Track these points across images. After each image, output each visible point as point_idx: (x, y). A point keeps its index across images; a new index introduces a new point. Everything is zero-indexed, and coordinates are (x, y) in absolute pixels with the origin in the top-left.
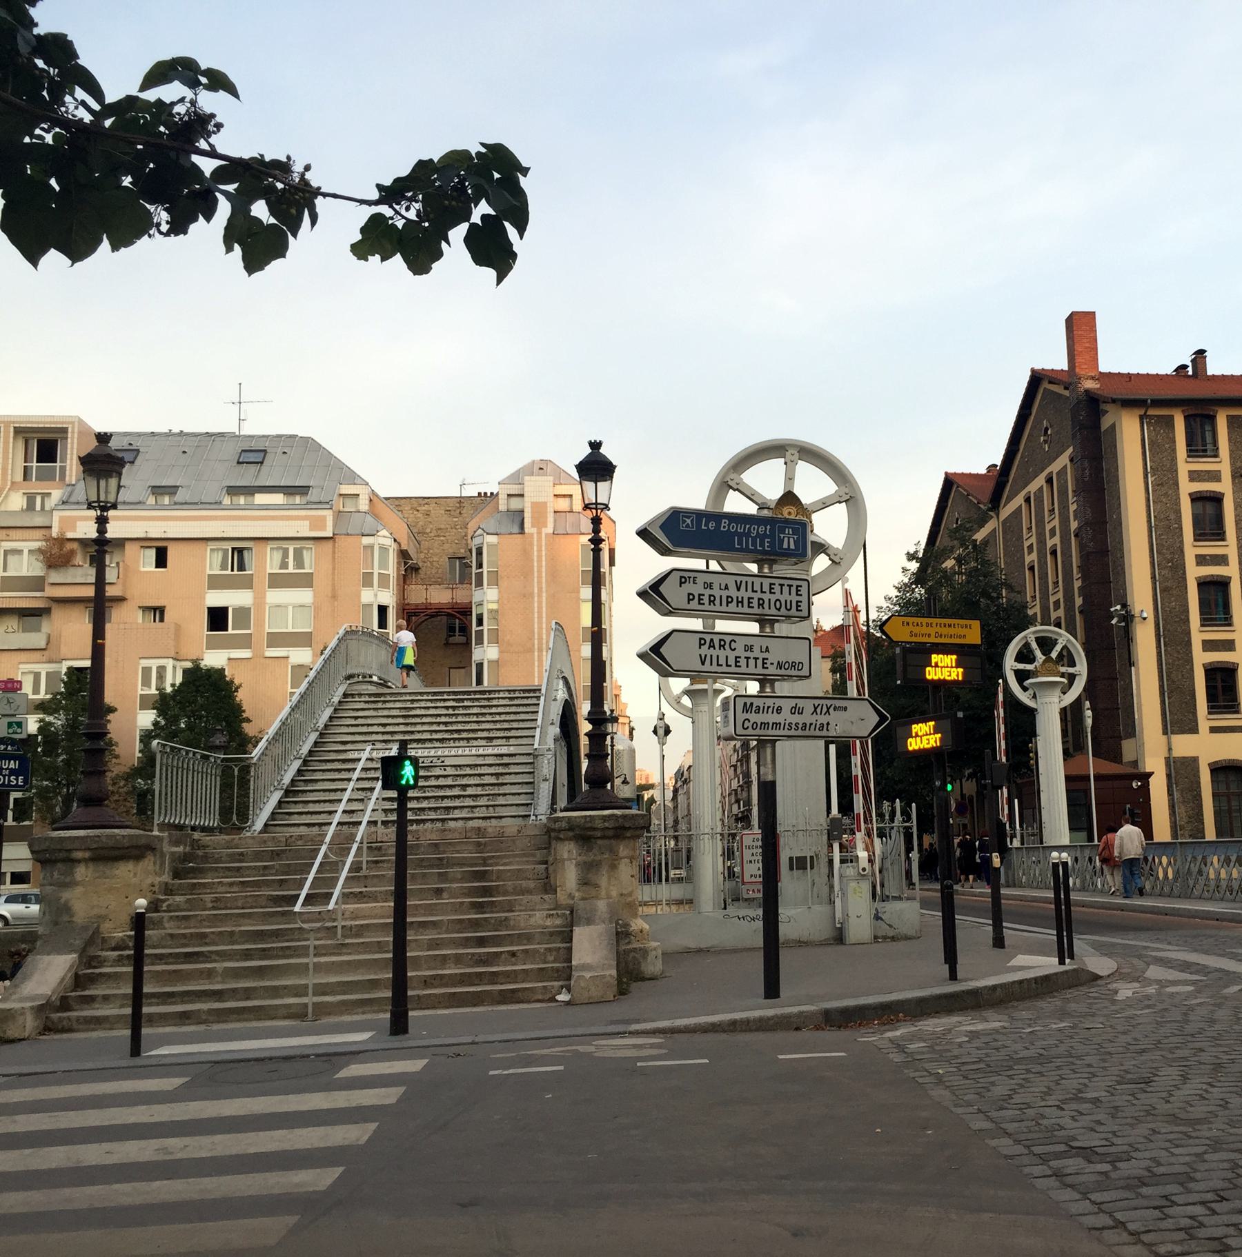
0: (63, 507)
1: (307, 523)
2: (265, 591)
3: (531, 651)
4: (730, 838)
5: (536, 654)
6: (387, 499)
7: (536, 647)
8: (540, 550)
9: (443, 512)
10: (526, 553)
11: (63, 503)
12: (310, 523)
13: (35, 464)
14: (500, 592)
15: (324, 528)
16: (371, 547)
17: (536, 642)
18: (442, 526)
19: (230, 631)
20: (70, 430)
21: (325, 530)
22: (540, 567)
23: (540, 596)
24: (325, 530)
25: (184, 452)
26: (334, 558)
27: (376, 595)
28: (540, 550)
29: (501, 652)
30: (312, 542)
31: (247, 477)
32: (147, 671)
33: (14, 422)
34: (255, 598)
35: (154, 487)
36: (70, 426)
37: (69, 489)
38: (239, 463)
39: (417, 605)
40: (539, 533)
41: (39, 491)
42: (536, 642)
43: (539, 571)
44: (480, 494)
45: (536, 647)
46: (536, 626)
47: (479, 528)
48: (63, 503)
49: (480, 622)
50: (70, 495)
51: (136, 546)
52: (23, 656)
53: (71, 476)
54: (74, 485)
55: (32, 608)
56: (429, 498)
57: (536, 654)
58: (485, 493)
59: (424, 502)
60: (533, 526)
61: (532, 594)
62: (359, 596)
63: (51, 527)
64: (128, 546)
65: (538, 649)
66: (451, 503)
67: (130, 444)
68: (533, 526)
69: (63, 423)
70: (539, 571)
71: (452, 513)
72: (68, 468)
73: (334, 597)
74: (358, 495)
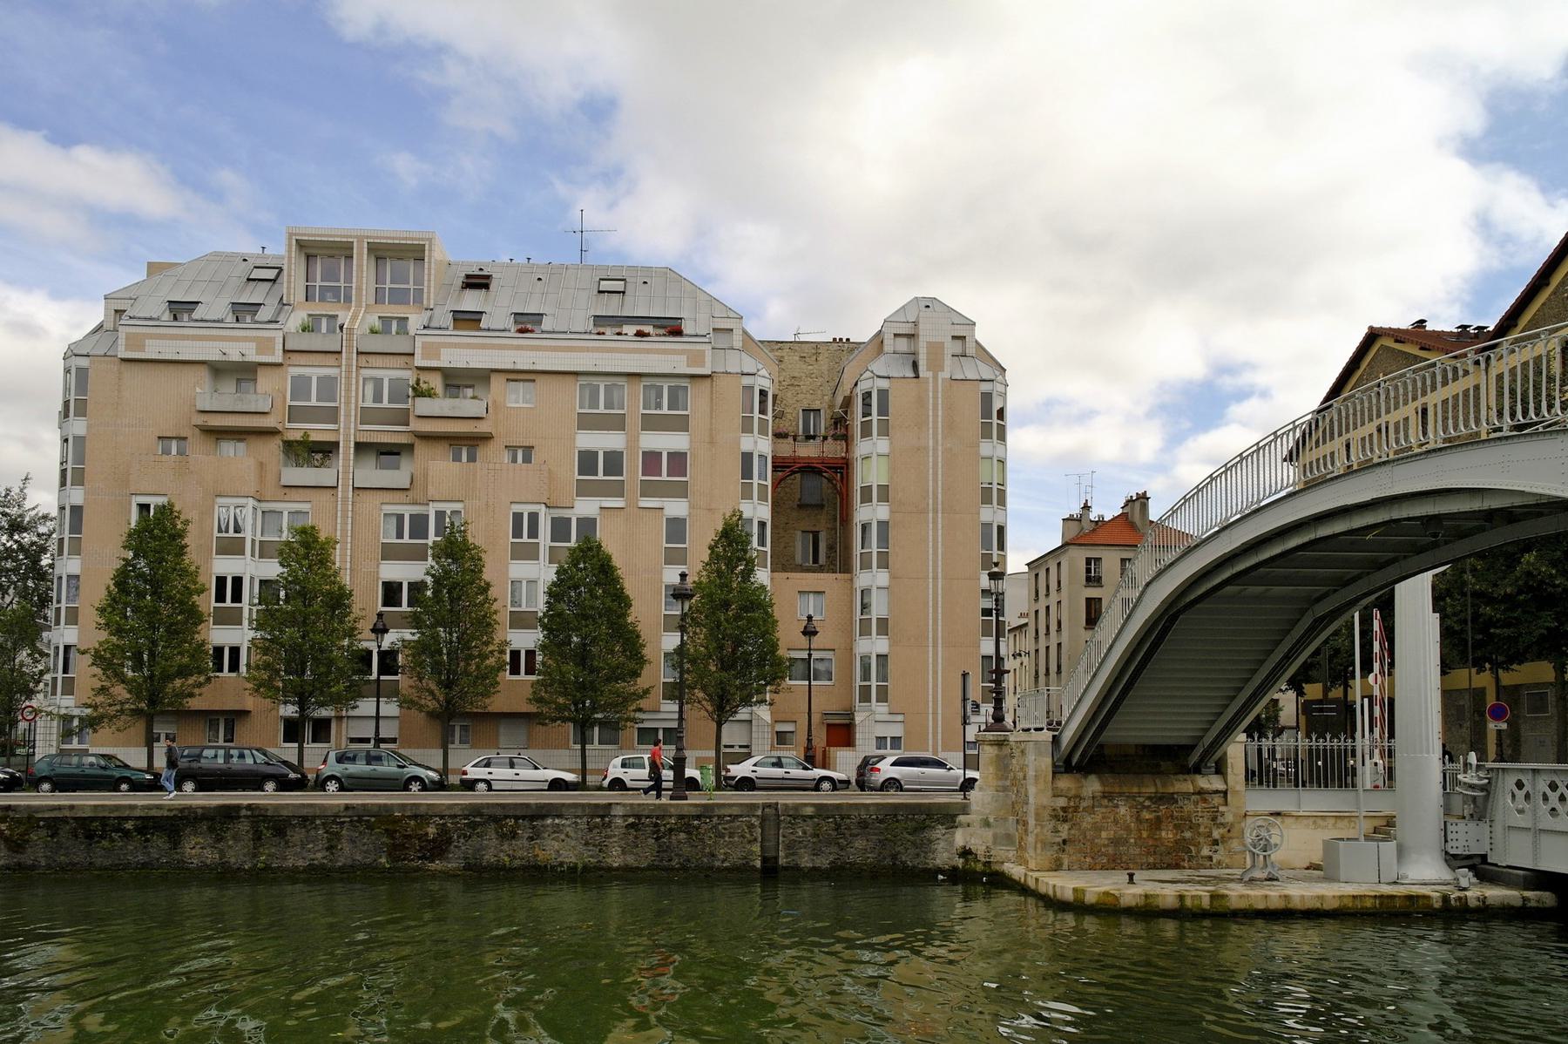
0: (425, 332)
1: (684, 358)
2: (639, 434)
3: (924, 511)
4: (774, 760)
5: (931, 515)
6: (762, 342)
7: (931, 507)
8: (935, 398)
9: (797, 358)
10: (921, 402)
11: (425, 327)
12: (688, 358)
13: (343, 286)
14: (891, 443)
15: (702, 365)
16: (751, 388)
17: (931, 502)
18: (796, 375)
19: (601, 476)
20: (427, 247)
21: (703, 366)
22: (935, 416)
23: (935, 449)
24: (703, 366)
25: (540, 279)
26: (712, 399)
27: (756, 442)
28: (935, 398)
29: (892, 512)
30: (688, 380)
31: (611, 307)
32: (518, 517)
33: (368, 237)
34: (628, 441)
35: (516, 314)
36: (355, 240)
37: (429, 313)
38: (600, 292)
39: (784, 458)
40: (935, 378)
41: (395, 315)
42: (931, 502)
43: (935, 422)
44: (835, 339)
45: (931, 507)
46: (931, 483)
47: (867, 370)
48: (425, 327)
49: (762, 488)
50: (430, 319)
51: (502, 378)
52: (388, 496)
53: (429, 299)
54: (432, 309)
55: (387, 444)
56: (782, 342)
57: (931, 515)
58: (841, 339)
59: (777, 347)
60: (928, 370)
61: (926, 448)
62: (739, 444)
63: (413, 354)
64: (494, 377)
65: (937, 512)
66: (807, 349)
67: (481, 269)
68: (928, 370)
69: (347, 236)
70: (935, 422)
71: (807, 360)
72: (425, 290)
73: (712, 442)
74: (732, 330)
